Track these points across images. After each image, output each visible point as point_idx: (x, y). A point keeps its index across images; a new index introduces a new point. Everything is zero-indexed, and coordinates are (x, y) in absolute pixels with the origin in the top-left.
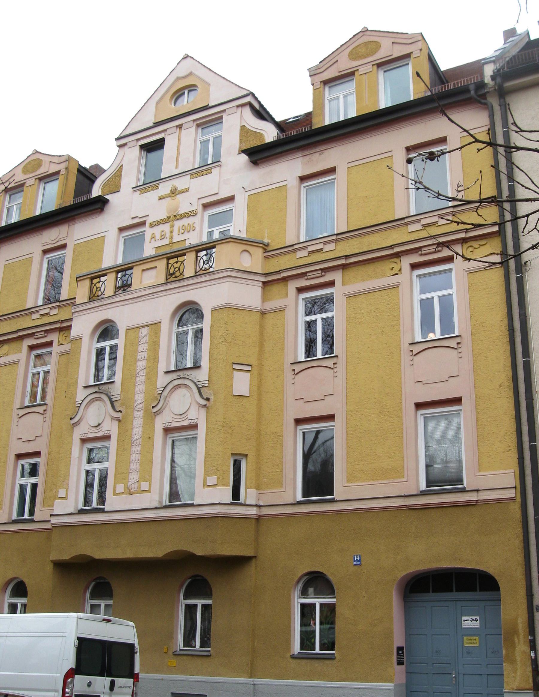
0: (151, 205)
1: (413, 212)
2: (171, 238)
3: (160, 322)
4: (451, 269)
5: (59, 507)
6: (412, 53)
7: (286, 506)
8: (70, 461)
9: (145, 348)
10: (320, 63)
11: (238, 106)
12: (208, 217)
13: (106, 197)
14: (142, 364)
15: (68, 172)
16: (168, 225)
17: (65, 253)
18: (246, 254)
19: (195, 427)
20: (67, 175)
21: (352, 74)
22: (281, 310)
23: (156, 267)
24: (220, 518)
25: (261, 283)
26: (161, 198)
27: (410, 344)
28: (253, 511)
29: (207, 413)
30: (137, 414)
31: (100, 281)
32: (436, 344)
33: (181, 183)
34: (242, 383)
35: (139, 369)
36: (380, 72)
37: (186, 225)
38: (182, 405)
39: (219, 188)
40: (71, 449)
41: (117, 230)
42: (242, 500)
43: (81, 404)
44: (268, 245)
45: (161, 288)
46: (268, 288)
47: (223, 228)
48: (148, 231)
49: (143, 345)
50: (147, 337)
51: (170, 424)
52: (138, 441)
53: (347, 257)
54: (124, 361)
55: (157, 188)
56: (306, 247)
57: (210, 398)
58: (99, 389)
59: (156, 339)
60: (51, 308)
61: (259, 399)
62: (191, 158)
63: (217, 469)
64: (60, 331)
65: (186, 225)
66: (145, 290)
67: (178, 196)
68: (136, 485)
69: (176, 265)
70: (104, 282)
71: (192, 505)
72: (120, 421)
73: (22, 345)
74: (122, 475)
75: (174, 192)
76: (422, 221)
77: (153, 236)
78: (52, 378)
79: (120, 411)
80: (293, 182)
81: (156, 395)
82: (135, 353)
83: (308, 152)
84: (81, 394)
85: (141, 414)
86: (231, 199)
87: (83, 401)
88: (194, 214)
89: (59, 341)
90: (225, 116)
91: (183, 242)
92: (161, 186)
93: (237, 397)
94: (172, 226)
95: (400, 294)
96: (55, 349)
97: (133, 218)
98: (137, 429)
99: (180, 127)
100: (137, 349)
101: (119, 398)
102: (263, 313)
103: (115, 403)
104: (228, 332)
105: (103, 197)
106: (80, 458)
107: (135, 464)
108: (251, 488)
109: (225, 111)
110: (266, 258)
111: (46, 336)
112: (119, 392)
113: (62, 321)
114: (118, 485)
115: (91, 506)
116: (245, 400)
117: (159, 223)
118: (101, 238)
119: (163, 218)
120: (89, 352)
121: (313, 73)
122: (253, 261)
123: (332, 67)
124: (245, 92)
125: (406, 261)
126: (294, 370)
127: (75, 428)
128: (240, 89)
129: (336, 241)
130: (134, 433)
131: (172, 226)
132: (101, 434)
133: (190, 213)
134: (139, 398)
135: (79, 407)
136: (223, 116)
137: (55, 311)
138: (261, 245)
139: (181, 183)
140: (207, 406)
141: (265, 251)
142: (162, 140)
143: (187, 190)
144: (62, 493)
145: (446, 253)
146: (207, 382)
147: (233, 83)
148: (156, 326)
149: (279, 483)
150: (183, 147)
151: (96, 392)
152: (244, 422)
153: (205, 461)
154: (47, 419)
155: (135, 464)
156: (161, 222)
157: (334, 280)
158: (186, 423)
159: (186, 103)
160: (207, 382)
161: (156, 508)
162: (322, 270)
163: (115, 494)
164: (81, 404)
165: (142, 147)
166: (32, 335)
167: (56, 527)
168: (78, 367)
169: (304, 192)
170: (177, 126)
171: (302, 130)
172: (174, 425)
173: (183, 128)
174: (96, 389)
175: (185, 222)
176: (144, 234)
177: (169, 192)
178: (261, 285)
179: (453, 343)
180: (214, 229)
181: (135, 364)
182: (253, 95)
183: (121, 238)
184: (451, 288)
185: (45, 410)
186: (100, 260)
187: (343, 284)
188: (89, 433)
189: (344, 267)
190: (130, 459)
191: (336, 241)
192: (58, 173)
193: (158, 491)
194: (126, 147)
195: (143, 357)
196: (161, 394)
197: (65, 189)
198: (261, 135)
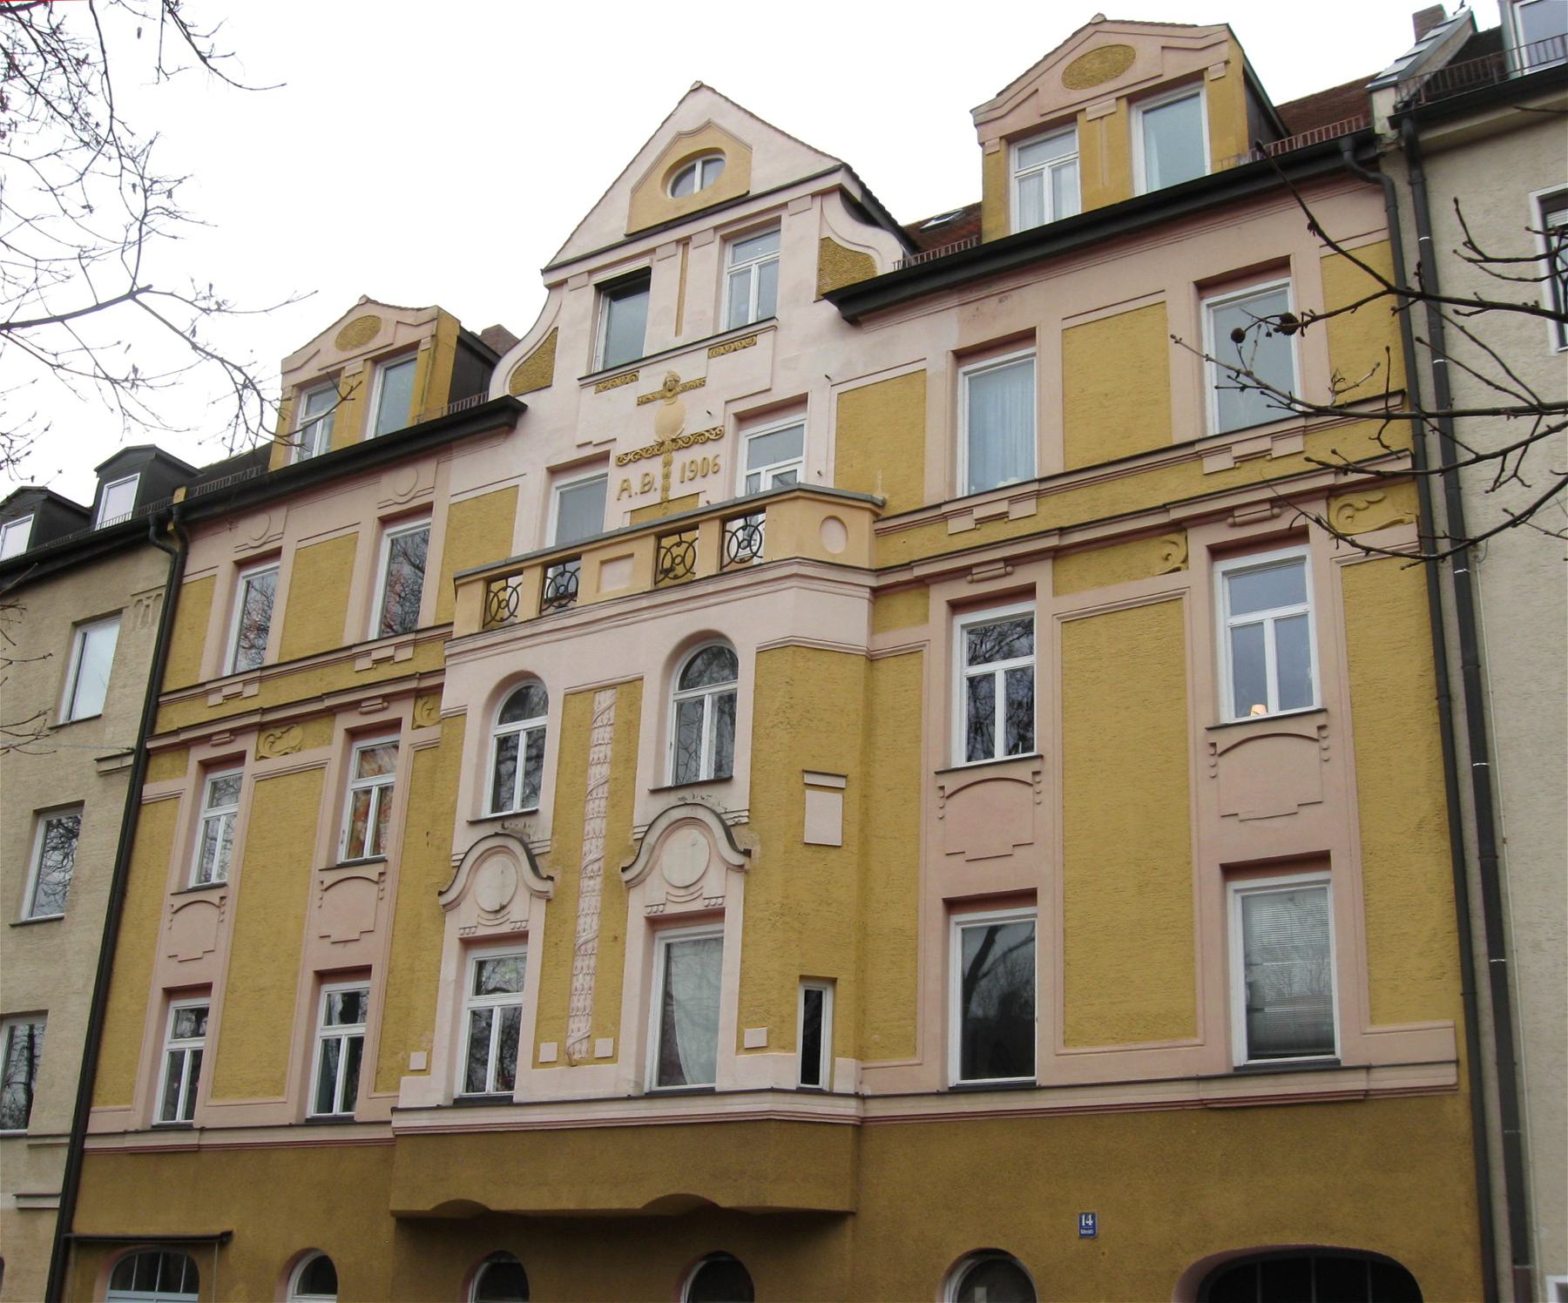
0: (620, 418)
2: (666, 489)
4: (1303, 558)
5: (413, 1092)
9: (607, 736)
11: (814, 195)
13: (522, 399)
14: (598, 773)
16: (659, 461)
18: (833, 525)
21: (1071, 119)
22: (914, 652)
23: (632, 555)
26: (643, 401)
28: (850, 1109)
29: (747, 883)
32: (1268, 732)
35: (592, 783)
37: (699, 461)
38: (689, 865)
42: (823, 1083)
44: (882, 505)
45: (645, 603)
47: (781, 466)
48: (615, 475)
52: (590, 945)
55: (635, 378)
56: (969, 510)
61: (864, 854)
62: (711, 313)
63: (767, 1012)
68: (584, 1046)
71: (710, 1092)
72: (549, 900)
74: (553, 1019)
75: (672, 388)
76: (1234, 447)
78: (397, 800)
79: (551, 878)
80: (938, 363)
81: (631, 842)
82: (586, 748)
84: (463, 838)
85: (596, 883)
86: (800, 402)
90: (784, 215)
91: (691, 500)
92: (643, 373)
94: (667, 464)
95: (1187, 612)
96: (406, 737)
98: (588, 920)
99: (685, 242)
100: (589, 739)
102: (872, 659)
103: (538, 860)
106: (459, 982)
108: (844, 1054)
109: (784, 205)
110: (879, 533)
111: (384, 709)
112: (548, 835)
116: (834, 854)
117: (638, 456)
118: (509, 491)
120: (483, 744)
122: (848, 540)
124: (830, 164)
125: (1199, 541)
126: (942, 788)
130: (580, 928)
131: (667, 464)
132: (506, 929)
134: (593, 850)
137: (407, 653)
138: (868, 505)
141: (878, 518)
142: (647, 271)
143: (701, 383)
144: (417, 1060)
145: (1020, 578)
147: (803, 144)
148: (630, 687)
149: (908, 1044)
150: (693, 287)
151: (497, 834)
154: (387, 894)
159: (699, 189)
165: (600, 288)
166: (355, 705)
168: (457, 779)
170: (678, 242)
172: (672, 909)
174: (497, 828)
175: (697, 453)
177: (660, 387)
180: (762, 469)
181: (586, 771)
182: (848, 169)
185: (381, 874)
186: (507, 541)
191: (1038, 494)
192: (414, 346)
194: (565, 289)
196: (642, 839)
198: (868, 257)
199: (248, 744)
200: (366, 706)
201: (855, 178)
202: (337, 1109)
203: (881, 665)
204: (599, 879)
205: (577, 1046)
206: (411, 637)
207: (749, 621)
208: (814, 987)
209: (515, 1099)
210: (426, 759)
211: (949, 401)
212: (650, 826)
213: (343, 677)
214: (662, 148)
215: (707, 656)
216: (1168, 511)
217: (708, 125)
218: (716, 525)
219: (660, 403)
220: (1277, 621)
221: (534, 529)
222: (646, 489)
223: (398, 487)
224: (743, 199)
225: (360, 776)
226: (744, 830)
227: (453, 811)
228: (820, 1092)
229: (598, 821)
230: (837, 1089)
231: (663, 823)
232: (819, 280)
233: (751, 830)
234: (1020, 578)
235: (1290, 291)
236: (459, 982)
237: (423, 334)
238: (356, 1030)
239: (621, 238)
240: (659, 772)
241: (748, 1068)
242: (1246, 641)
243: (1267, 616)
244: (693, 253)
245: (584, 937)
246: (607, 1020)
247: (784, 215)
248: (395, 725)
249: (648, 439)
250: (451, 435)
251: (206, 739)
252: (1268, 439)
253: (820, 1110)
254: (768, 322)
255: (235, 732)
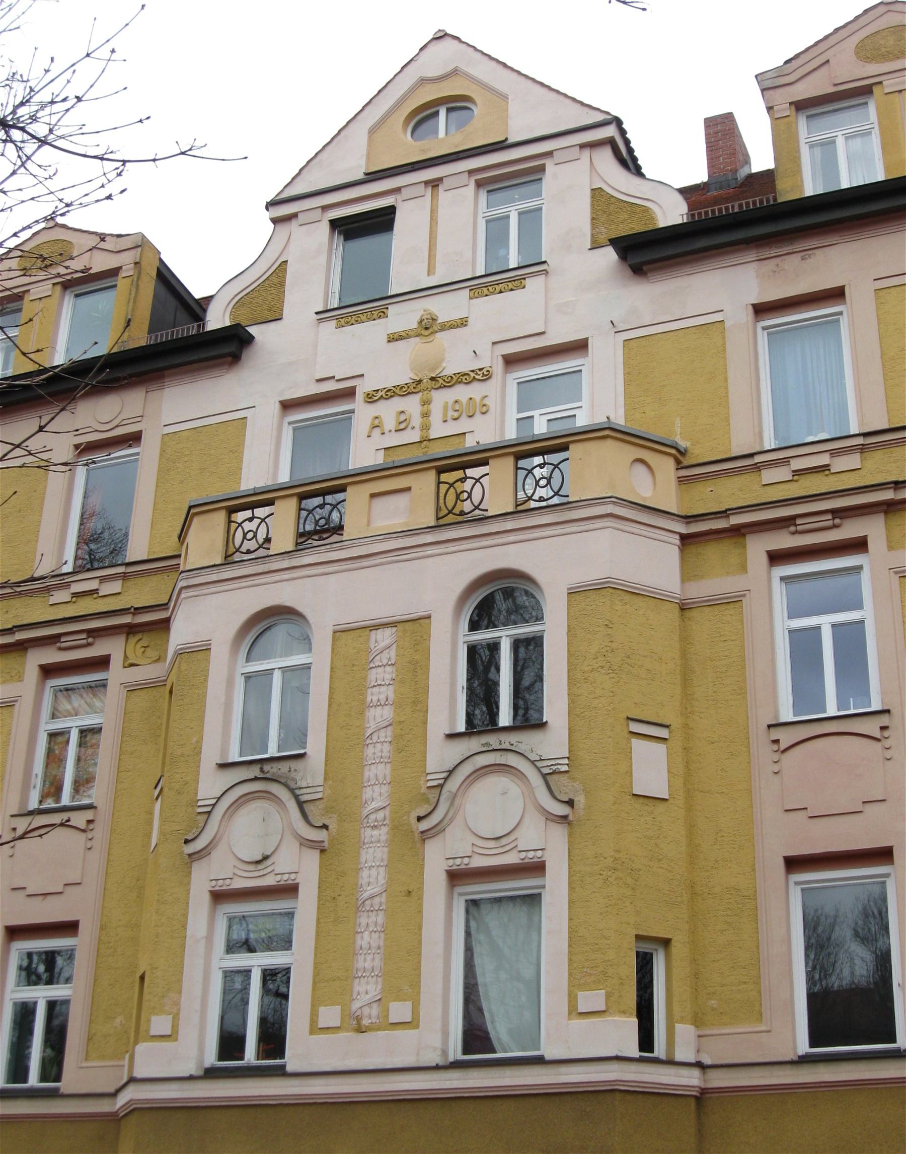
0: (369, 354)
1: (769, 443)
2: (426, 427)
3: (429, 617)
4: (861, 567)
5: (149, 1060)
6: (121, 268)
7: (776, 1067)
8: (183, 946)
9: (388, 677)
10: (787, 62)
11: (582, 146)
12: (515, 385)
13: (251, 330)
14: (378, 716)
15: (139, 274)
16: (415, 400)
17: (138, 454)
18: (641, 469)
19: (290, 890)
20: (138, 279)
21: (866, 91)
22: (734, 601)
23: (409, 489)
24: (618, 1095)
25: (678, 537)
26: (393, 338)
27: (12, 816)
28: (692, 1079)
29: (570, 835)
30: (368, 834)
31: (466, 478)
32: (840, 728)
33: (446, 307)
34: (651, 768)
35: (372, 726)
36: (67, 298)
37: (464, 400)
38: (498, 814)
39: (546, 322)
40: (185, 916)
41: (278, 406)
42: (660, 1050)
43: (214, 805)
44: (683, 453)
45: (429, 538)
46: (692, 549)
47: (559, 409)
48: (363, 413)
49: (380, 670)
50: (393, 652)
51: (466, 860)
52: (377, 900)
53: (138, 610)
54: (330, 705)
55: (383, 314)
56: (786, 461)
57: (576, 799)
58: (262, 771)
59: (417, 657)
60: (103, 579)
61: (689, 808)
62: (468, 254)
63: (604, 973)
64: (128, 634)
65: (464, 400)
66: (381, 541)
67: (439, 335)
68: (375, 1010)
69: (247, 526)
70: (263, 520)
71: (539, 1061)
72: (323, 851)
73: (24, 663)
74: (332, 981)
75: (428, 327)
76: (792, 461)
77: (377, 422)
78: (107, 743)
79: (325, 827)
80: (737, 314)
81: (423, 790)
82: (361, 688)
83: (773, 252)
84: (210, 784)
85: (382, 833)
86: (580, 347)
87: (219, 799)
88: (485, 376)
89: (126, 657)
90: (549, 164)
91: (457, 440)
92: (392, 310)
93: (641, 800)
94: (426, 403)
95: (16, 716)
96: (116, 674)
97: (319, 381)
98: (374, 872)
99: (434, 184)
100: (365, 678)
101: (320, 796)
102: (684, 608)
103: (308, 808)
104: (614, 645)
105: (243, 328)
106: (209, 938)
107: (369, 958)
108: (682, 1020)
109: (550, 154)
110: (681, 480)
111: (89, 645)
112: (320, 780)
113: (136, 609)
114: (322, 1009)
115: (242, 1058)
116: (661, 807)
117: (390, 393)
118: (244, 421)
119: (402, 382)
120: (230, 683)
121: (769, 83)
122: (656, 485)
123: (815, 74)
124: (600, 117)
125: (757, 548)
126: (776, 742)
127: (196, 866)
128: (586, 110)
129: (862, 449)
130: (364, 881)
131: (426, 403)
132: (270, 881)
133: (472, 374)
134: (376, 797)
135: (209, 813)
136: (544, 165)
137: (115, 587)
138: (673, 451)
139: (446, 307)
140: (571, 818)
141: (679, 466)
142: (391, 211)
143: (463, 323)
144: (160, 1024)
145: (850, 530)
146: (566, 761)
147: (566, 96)
148: (415, 626)
149: (752, 1009)
150: (443, 229)
151: (256, 779)
152: (660, 860)
153: (569, 952)
154: (96, 844)
155: (369, 958)
156: (397, 391)
157: (109, 655)
158: (512, 859)
159: (445, 135)
160: (566, 761)
161: (437, 1068)
162: (835, 512)
163: (315, 1029)
164: (214, 805)
165: (335, 224)
166: (54, 639)
167: (135, 1110)
168: (201, 718)
169: (763, 339)
170: (427, 183)
171: (768, 201)
172: (478, 862)
173: (441, 188)
174: (254, 771)
175: (461, 393)
176: (350, 418)
177: (415, 325)
178: (678, 542)
179: (871, 727)
180: (535, 413)
181: (362, 713)
182: (618, 122)
183: (285, 425)
184: (859, 606)
185: (90, 822)
186: (236, 473)
187: (890, 548)
188: (236, 879)
189: (130, 630)
190: (354, 942)
191: (862, 449)
192: (114, 272)
193: (438, 1026)
194: (294, 223)
195: (382, 697)
196: (441, 786)
197: (133, 310)
198: (647, 210)
199: (113, 647)
200: (66, 641)
201: (623, 132)
202: (33, 1079)
203: (694, 613)
204: (384, 830)
205: (366, 1011)
206: (121, 569)
207: (557, 563)
208: (646, 947)
209: (289, 1068)
210: (141, 700)
211: (753, 353)
212: (451, 772)
213: (35, 610)
214: (402, 92)
215: (500, 599)
216: (14, 633)
217: (455, 72)
218: (221, 516)
219: (414, 341)
220: (834, 626)
221: (267, 459)
222: (402, 426)
223: (99, 414)
224: (501, 146)
225: (54, 716)
226: (563, 779)
227: (197, 752)
228: (656, 1061)
229: (381, 767)
230: (679, 1057)
231: (467, 769)
232: (593, 229)
233: (573, 779)
234: (850, 530)
235: (844, 321)
236: (209, 938)
237: (126, 260)
238: (57, 992)
239: (360, 176)
240: (225, 749)
241: (578, 1033)
242: (805, 646)
243: (825, 622)
244: (443, 196)
245: (369, 891)
246: (403, 977)
247: (549, 164)
248: (103, 663)
249: (404, 377)
250: (160, 364)
251: (54, 639)
252: (827, 455)
253: (647, 1078)
254: (535, 266)
255: (840, 513)
